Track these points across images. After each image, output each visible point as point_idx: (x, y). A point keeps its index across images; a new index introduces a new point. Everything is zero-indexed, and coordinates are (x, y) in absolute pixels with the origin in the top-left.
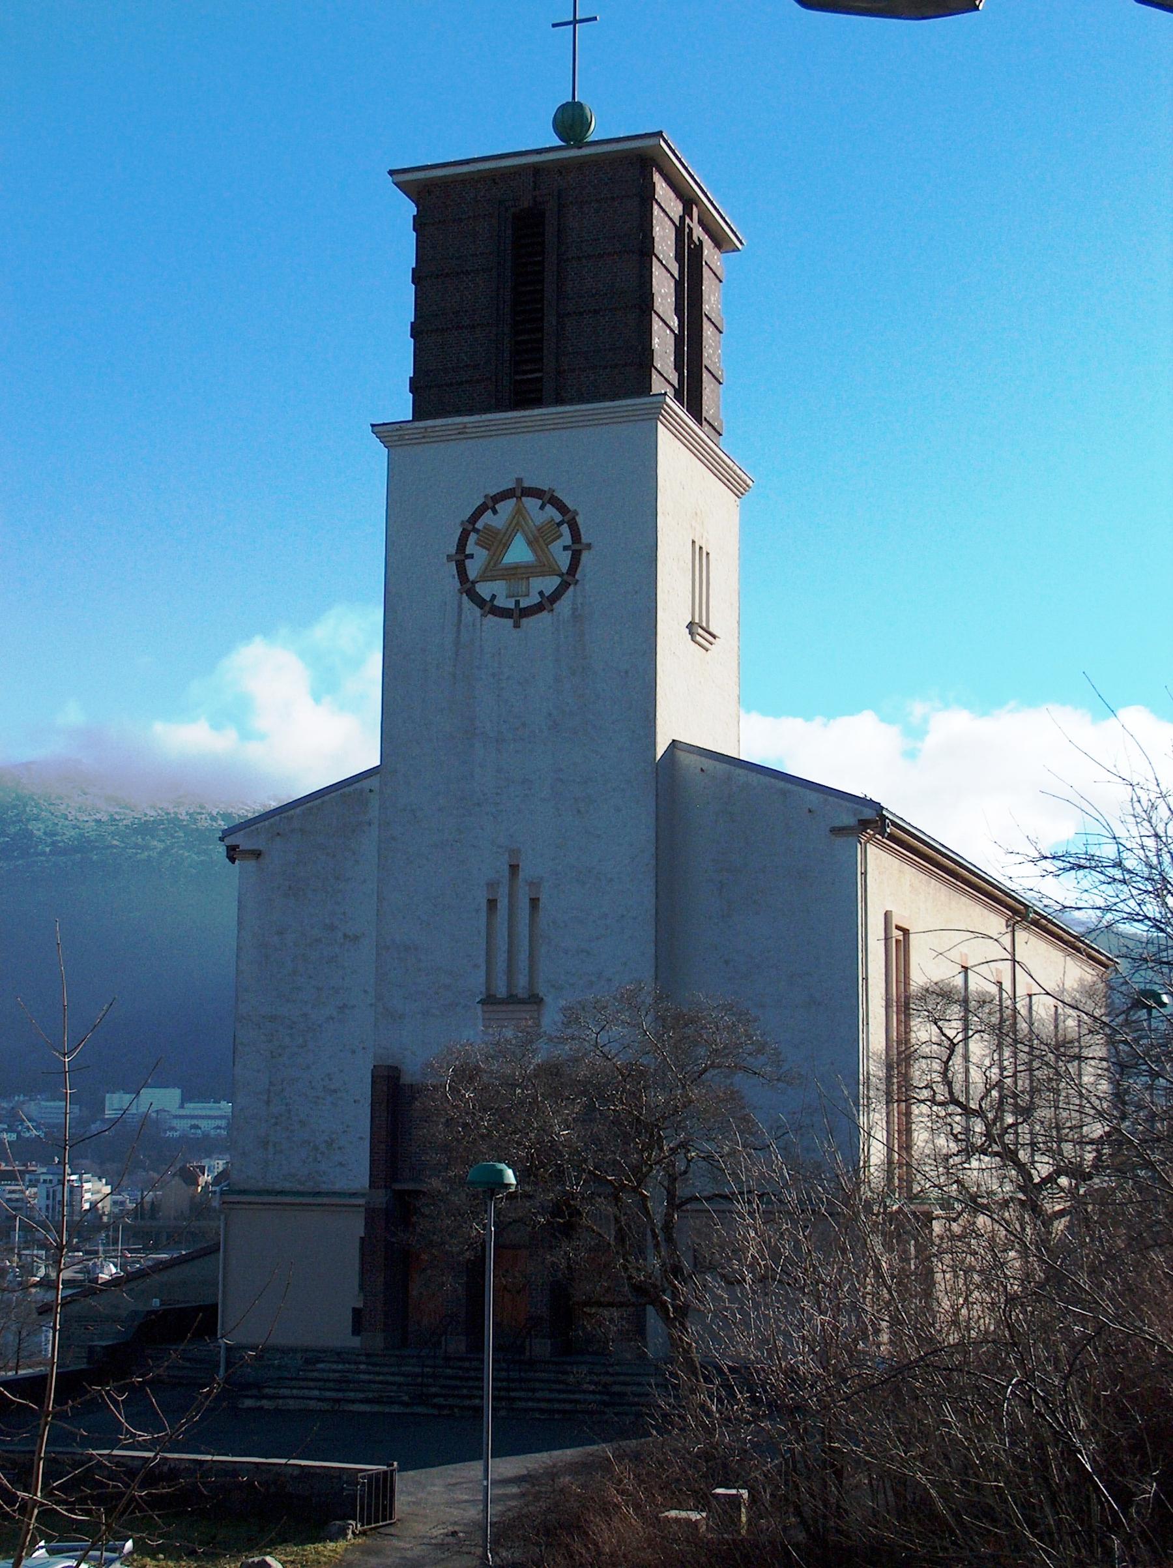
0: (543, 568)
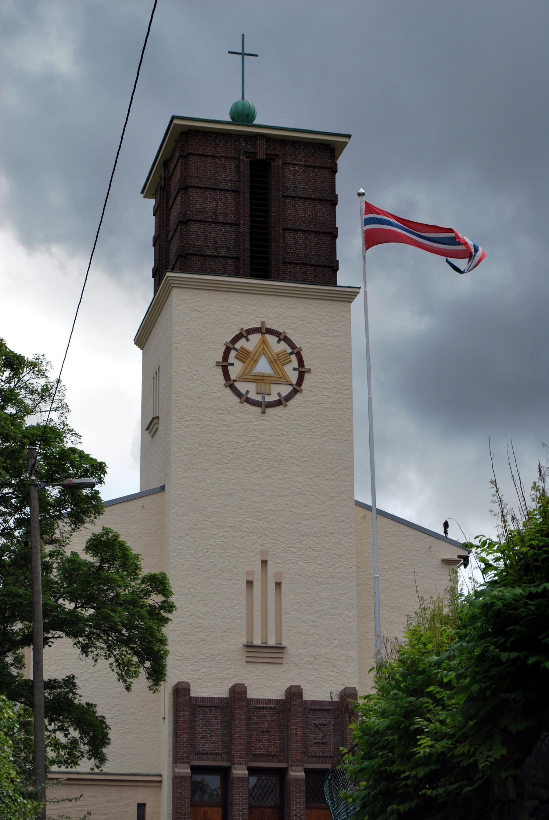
0: (283, 380)
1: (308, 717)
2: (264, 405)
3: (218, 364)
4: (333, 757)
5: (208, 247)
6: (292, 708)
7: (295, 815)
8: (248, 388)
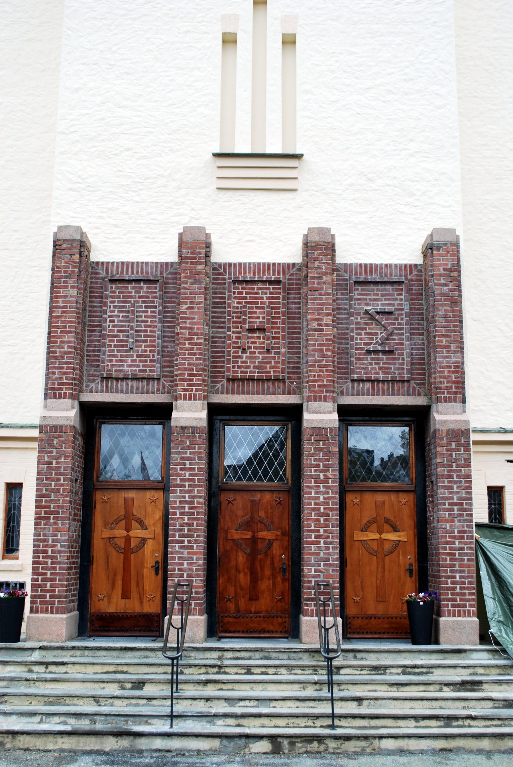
1: (351, 299)
4: (408, 381)
6: (310, 275)
7: (313, 510)
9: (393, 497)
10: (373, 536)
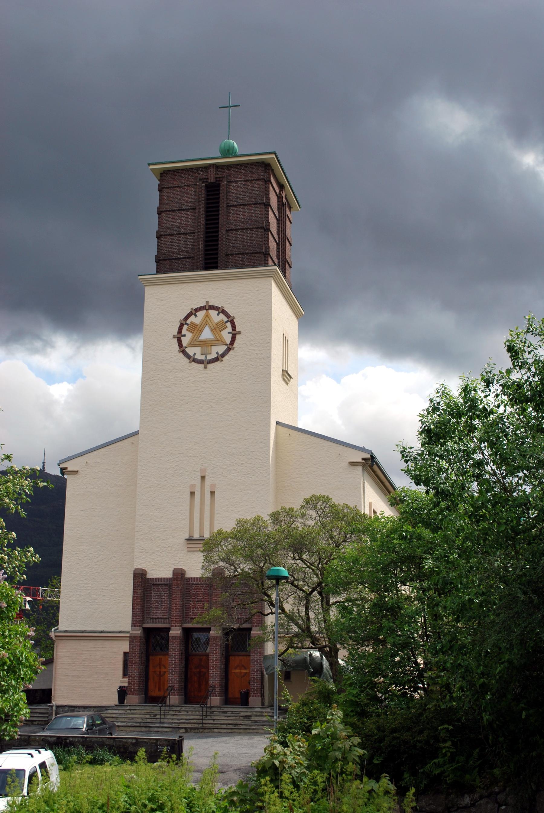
0: (219, 341)
2: (205, 362)
3: (174, 336)
5: (173, 253)
8: (195, 351)
9: (245, 657)
10: (238, 671)
